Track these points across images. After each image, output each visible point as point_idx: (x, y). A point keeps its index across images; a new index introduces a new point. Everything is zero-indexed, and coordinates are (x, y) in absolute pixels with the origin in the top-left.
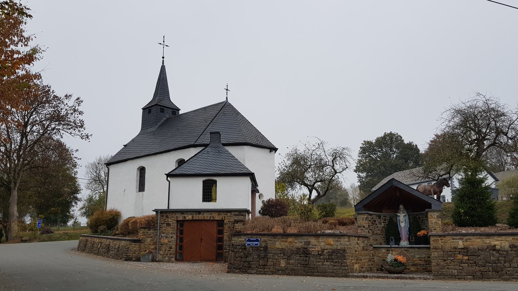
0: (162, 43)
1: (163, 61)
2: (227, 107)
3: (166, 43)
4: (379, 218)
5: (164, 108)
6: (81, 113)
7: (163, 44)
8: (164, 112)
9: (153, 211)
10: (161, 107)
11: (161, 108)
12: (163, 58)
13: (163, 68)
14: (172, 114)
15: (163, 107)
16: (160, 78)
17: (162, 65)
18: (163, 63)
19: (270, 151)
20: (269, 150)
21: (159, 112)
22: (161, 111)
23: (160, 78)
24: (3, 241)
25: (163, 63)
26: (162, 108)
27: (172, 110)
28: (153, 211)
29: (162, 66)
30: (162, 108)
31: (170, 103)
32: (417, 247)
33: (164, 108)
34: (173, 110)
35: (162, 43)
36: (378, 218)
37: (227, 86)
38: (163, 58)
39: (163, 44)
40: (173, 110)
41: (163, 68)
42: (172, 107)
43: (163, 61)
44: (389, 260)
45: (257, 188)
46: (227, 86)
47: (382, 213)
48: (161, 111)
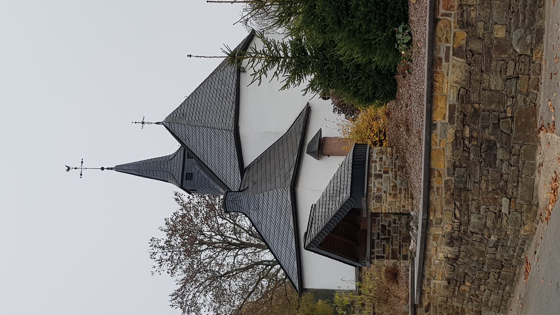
0: (78, 171)
1: (108, 169)
3: (79, 165)
4: (377, 217)
5: (185, 174)
7: (81, 168)
8: (191, 174)
9: (266, 76)
10: (184, 179)
11: (186, 179)
12: (103, 169)
13: (120, 169)
14: (191, 179)
15: (183, 176)
18: (111, 169)
21: (192, 182)
22: (191, 179)
25: (111, 169)
26: (185, 177)
28: (266, 76)
30: (185, 177)
31: (179, 157)
33: (185, 174)
34: (186, 157)
35: (78, 171)
36: (378, 219)
37: (136, 123)
38: (103, 169)
40: (186, 157)
41: (120, 169)
42: (182, 159)
43: (108, 169)
45: (355, 289)
46: (136, 123)
47: (367, 230)
48: (189, 174)
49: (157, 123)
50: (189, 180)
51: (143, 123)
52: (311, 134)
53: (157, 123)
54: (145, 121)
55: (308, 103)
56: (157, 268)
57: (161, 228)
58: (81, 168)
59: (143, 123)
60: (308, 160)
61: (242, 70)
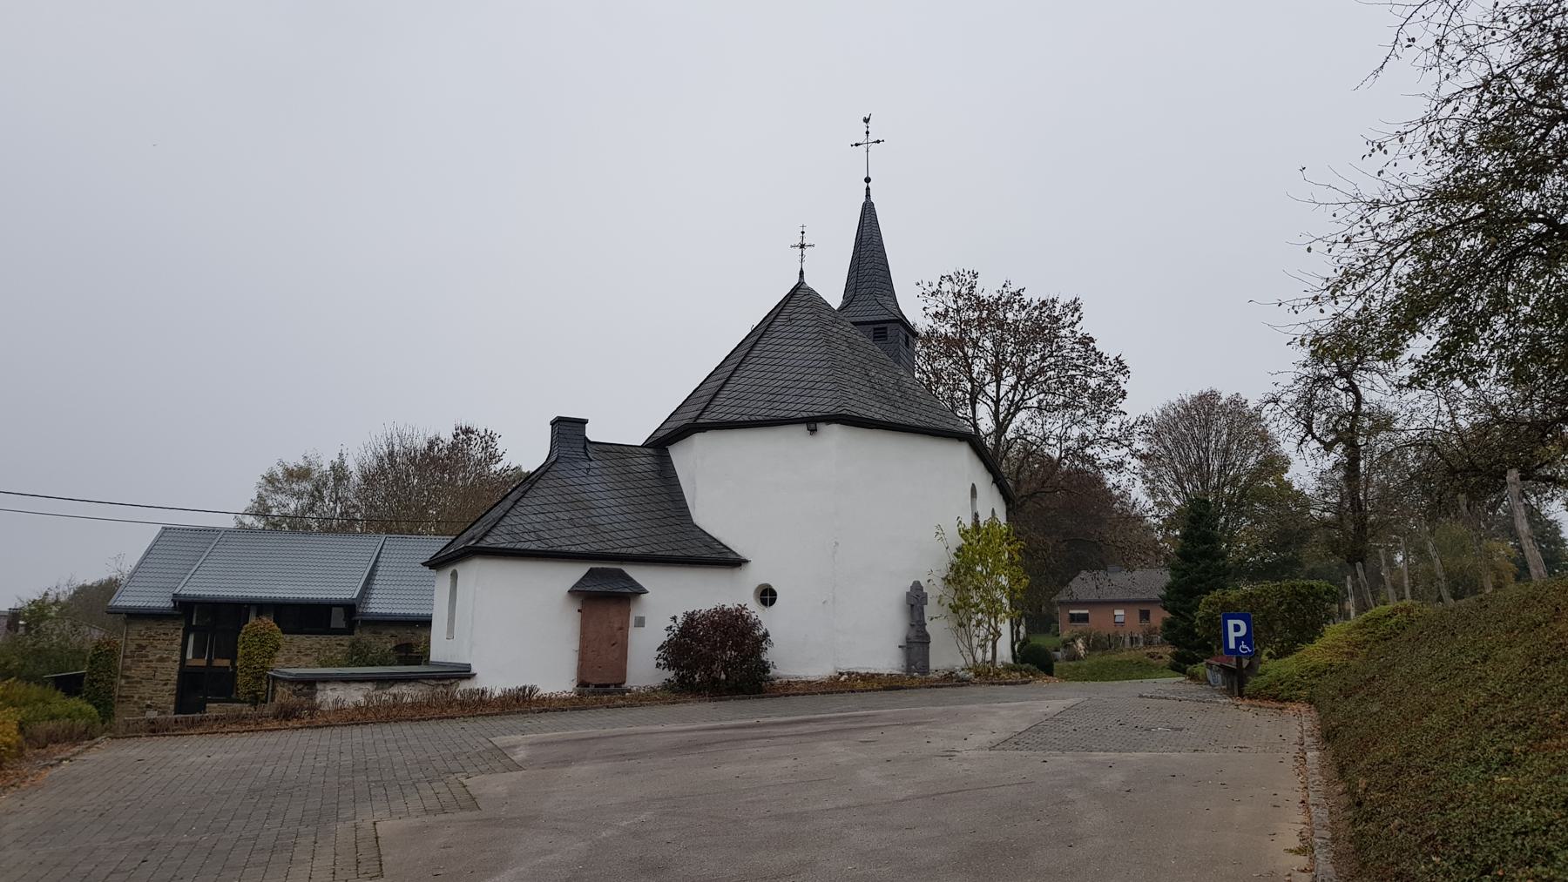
1: (868, 189)
2: (777, 329)
6: (663, 669)
11: (875, 329)
12: (868, 180)
13: (868, 211)
14: (875, 337)
16: (861, 239)
17: (864, 201)
18: (868, 195)
19: (813, 431)
20: (804, 427)
23: (861, 239)
24: (1259, 672)
25: (868, 195)
26: (881, 326)
27: (872, 326)
29: (865, 205)
30: (881, 326)
32: (839, 718)
33: (885, 325)
34: (876, 326)
35: (872, 138)
37: (803, 233)
38: (868, 180)
39: (868, 142)
40: (876, 326)
41: (868, 211)
42: (872, 319)
43: (868, 189)
44: (1110, 482)
46: (803, 233)
49: (802, 273)
50: (886, 333)
51: (802, 246)
52: (638, 574)
53: (802, 273)
54: (807, 251)
55: (746, 561)
56: (930, 289)
57: (1008, 284)
58: (868, 142)
59: (802, 246)
60: (575, 573)
61: (813, 426)
